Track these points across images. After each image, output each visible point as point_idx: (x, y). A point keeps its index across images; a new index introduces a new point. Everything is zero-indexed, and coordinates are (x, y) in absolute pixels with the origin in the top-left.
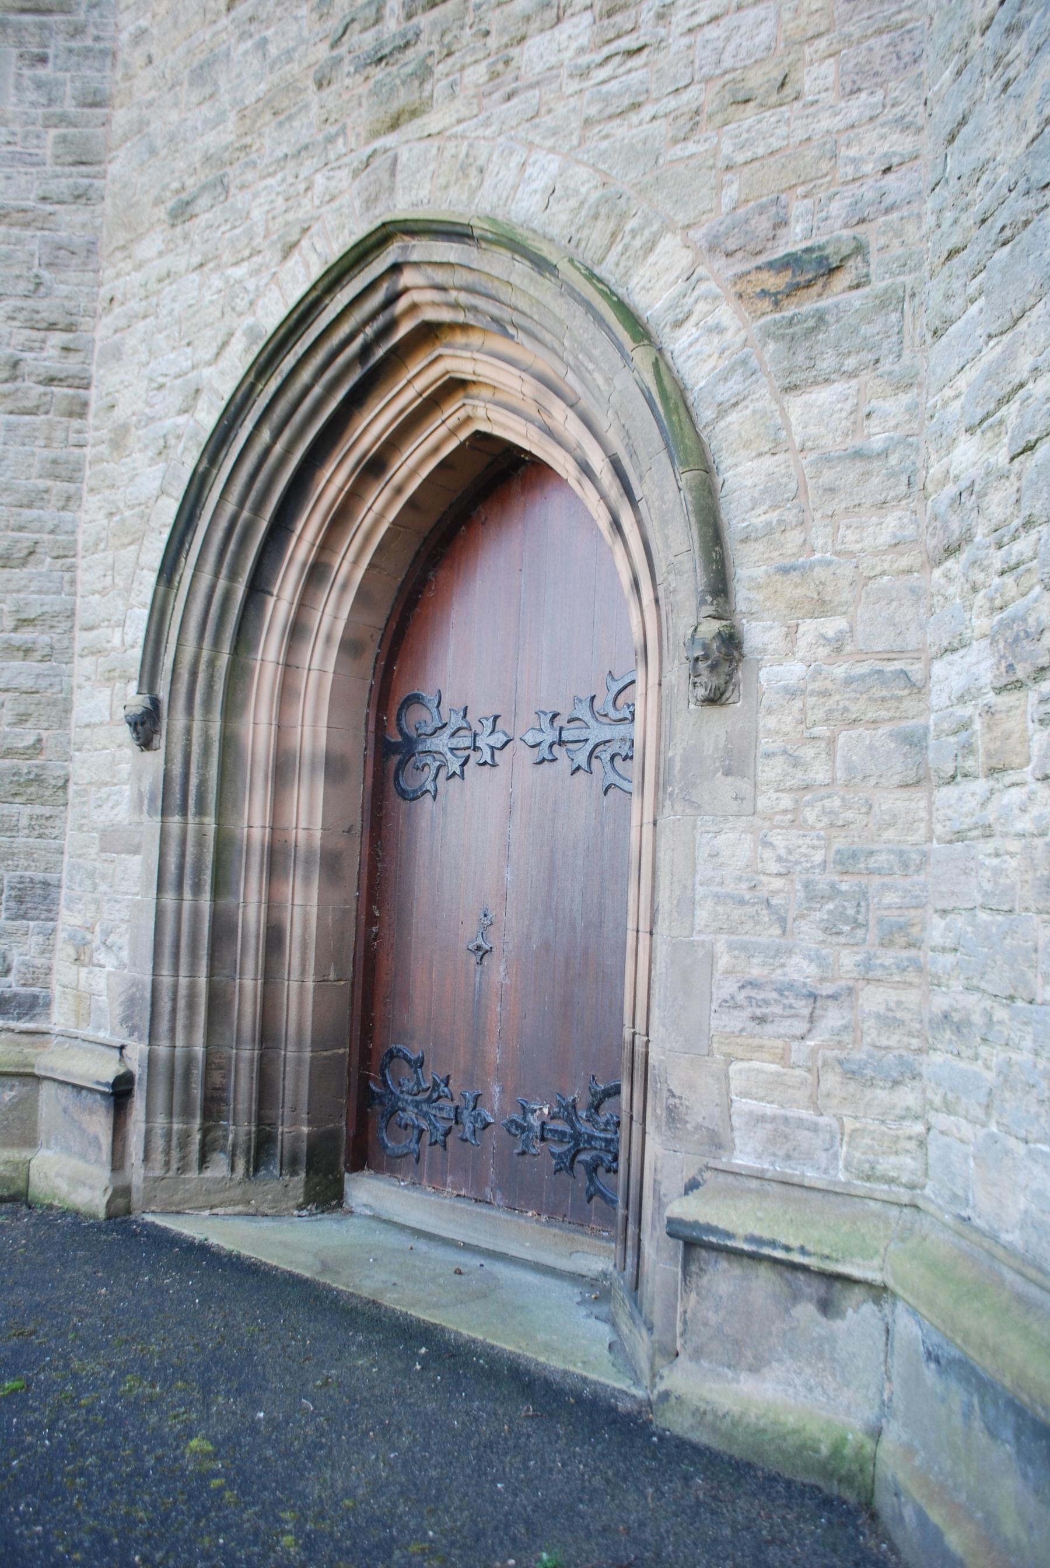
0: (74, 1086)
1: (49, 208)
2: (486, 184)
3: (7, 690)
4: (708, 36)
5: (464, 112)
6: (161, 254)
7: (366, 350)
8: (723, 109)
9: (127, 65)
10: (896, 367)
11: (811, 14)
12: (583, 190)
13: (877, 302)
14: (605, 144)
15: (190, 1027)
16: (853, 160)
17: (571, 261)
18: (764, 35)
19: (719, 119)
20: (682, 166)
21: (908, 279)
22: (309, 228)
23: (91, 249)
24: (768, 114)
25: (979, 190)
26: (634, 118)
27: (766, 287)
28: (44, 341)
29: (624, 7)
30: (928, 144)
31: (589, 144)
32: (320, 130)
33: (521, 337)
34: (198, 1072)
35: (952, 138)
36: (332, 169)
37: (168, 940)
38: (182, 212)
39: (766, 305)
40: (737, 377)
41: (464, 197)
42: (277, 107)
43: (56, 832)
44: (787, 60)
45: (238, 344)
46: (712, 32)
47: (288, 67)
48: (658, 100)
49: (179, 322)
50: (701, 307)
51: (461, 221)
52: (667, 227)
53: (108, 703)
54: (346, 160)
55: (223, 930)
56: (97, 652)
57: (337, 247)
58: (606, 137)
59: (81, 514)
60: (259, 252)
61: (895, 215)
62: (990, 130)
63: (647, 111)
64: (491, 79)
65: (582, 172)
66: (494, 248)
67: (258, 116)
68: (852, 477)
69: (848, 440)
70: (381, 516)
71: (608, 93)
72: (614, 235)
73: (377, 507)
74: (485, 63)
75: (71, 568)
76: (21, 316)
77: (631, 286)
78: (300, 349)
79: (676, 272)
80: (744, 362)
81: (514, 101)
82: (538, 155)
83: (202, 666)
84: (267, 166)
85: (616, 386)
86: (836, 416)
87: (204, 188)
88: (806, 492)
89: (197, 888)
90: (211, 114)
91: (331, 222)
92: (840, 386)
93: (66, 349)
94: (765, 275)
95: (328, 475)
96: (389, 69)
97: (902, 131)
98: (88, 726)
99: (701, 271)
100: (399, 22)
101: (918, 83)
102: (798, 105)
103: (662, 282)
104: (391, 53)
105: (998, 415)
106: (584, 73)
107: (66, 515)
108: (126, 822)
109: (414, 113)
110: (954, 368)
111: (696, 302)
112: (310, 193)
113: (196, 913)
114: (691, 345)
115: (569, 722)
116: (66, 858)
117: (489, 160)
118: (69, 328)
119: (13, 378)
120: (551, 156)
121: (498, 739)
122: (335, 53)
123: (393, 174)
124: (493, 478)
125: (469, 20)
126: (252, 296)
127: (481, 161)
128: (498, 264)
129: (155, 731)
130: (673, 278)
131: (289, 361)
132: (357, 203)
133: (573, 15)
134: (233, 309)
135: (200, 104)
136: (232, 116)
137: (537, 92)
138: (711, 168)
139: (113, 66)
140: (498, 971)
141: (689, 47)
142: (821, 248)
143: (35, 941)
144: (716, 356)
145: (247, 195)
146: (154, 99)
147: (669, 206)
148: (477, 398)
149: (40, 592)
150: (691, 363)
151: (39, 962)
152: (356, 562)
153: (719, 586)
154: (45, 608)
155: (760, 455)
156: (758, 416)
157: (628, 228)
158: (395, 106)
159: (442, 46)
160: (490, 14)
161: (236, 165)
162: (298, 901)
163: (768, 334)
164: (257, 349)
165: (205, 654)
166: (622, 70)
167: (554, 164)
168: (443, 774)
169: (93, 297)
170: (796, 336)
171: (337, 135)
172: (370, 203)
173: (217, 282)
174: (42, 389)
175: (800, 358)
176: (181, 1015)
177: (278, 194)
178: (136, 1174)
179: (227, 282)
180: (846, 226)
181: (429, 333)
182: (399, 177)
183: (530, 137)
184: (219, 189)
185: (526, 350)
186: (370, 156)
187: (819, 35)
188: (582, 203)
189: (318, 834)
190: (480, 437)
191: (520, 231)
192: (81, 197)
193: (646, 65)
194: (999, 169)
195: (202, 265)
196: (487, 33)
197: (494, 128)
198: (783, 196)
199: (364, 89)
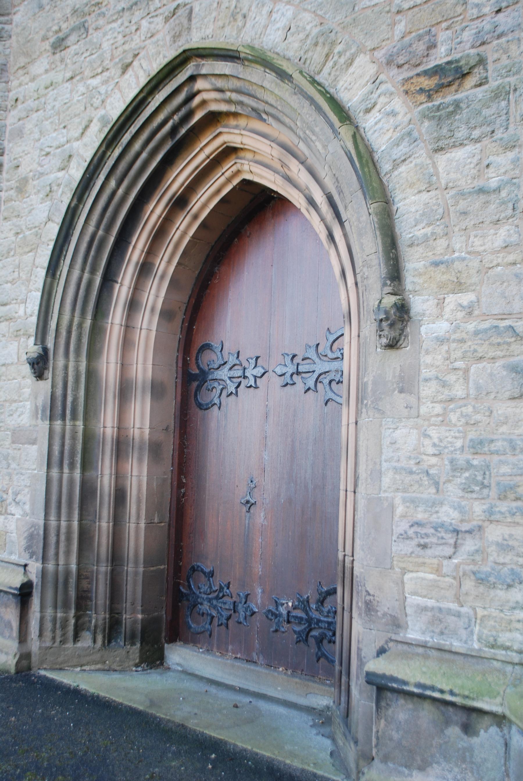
2: (248, 25)
6: (47, 71)
10: (505, 135)
12: (308, 27)
13: (493, 94)
15: (68, 553)
17: (301, 72)
20: (370, 11)
22: (138, 54)
33: (271, 120)
34: (73, 581)
36: (152, 17)
37: (54, 498)
38: (59, 45)
39: (423, 98)
40: (405, 143)
41: (234, 33)
45: (95, 127)
51: (232, 48)
52: (360, 50)
54: (161, 11)
55: (88, 492)
57: (156, 65)
60: (108, 69)
61: (503, 40)
65: (307, 16)
66: (253, 65)
68: (477, 205)
70: (185, 233)
72: (327, 56)
77: (338, 87)
78: (133, 129)
80: (409, 134)
83: (74, 328)
84: (112, 15)
85: (330, 150)
86: (467, 167)
87: (73, 30)
88: (449, 214)
92: (470, 148)
94: (422, 79)
95: (151, 208)
103: (357, 85)
108: (28, 425)
111: (379, 96)
112: (138, 32)
113: (71, 481)
114: (376, 124)
115: (303, 360)
120: (288, 7)
121: (259, 371)
123: (190, 19)
126: (103, 97)
127: (244, 11)
128: (256, 75)
131: (127, 137)
132: (168, 38)
134: (92, 105)
138: (388, 12)
140: (260, 517)
142: (457, 61)
144: (392, 130)
145: (100, 33)
147: (361, 37)
150: (376, 135)
152: (169, 262)
153: (395, 274)
155: (420, 192)
156: (418, 168)
157: (336, 51)
161: (93, 15)
162: (135, 473)
163: (424, 116)
164: (106, 130)
172: (176, 37)
173: (81, 88)
176: (62, 545)
177: (119, 33)
178: (34, 645)
179: (88, 88)
180: (473, 47)
181: (213, 119)
182: (194, 21)
184: (82, 30)
186: (175, 9)
188: (308, 36)
189: (147, 431)
190: (245, 183)
191: (269, 54)
195: (72, 78)
198: (433, 29)
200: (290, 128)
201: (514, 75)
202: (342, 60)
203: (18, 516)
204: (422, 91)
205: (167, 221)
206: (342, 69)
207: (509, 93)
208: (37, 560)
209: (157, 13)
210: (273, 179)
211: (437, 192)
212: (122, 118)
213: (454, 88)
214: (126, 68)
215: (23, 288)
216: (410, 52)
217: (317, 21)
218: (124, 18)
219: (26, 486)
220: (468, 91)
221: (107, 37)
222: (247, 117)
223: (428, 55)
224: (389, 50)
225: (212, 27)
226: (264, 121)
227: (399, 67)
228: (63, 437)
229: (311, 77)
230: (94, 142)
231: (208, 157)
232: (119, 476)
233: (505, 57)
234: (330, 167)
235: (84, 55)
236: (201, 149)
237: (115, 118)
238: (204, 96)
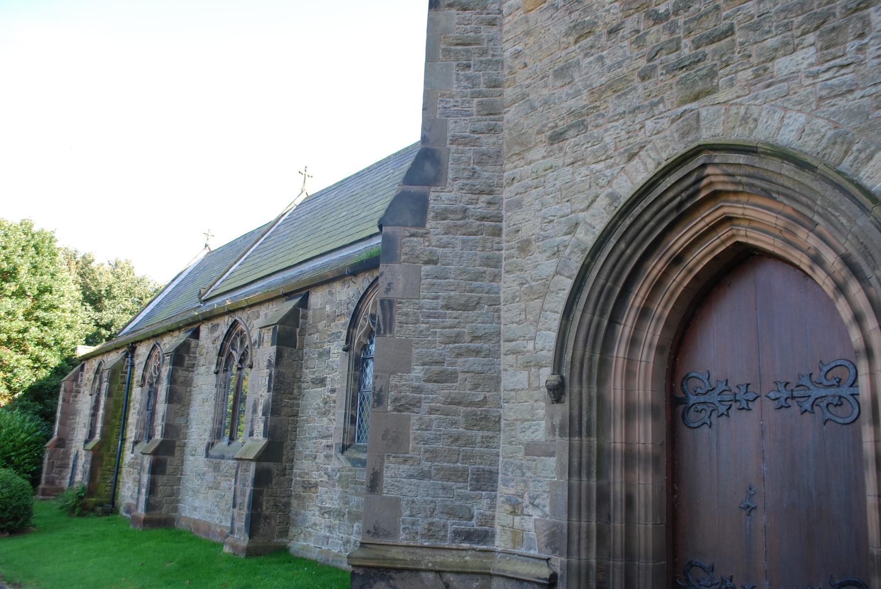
0: (517, 580)
1: (477, 136)
3: (468, 372)
5: (740, 93)
6: (544, 157)
9: (511, 68)
12: (823, 130)
14: (833, 109)
15: (588, 549)
23: (499, 154)
26: (850, 97)
28: (477, 200)
29: (836, 45)
34: (593, 573)
37: (575, 502)
38: (557, 137)
42: (617, 87)
43: (495, 445)
45: (602, 202)
49: (560, 190)
53: (526, 379)
55: (603, 497)
56: (515, 352)
58: (833, 105)
59: (502, 284)
63: (858, 94)
65: (822, 122)
67: (604, 92)
70: (680, 284)
71: (832, 85)
73: (678, 280)
75: (498, 310)
76: (467, 188)
83: (586, 361)
89: (589, 475)
93: (489, 203)
96: (687, 73)
98: (513, 390)
100: (691, 50)
104: (689, 65)
106: (815, 75)
107: (494, 284)
108: (543, 440)
109: (708, 93)
112: (643, 130)
113: (589, 488)
115: (797, 387)
116: (501, 459)
118: (490, 193)
119: (464, 218)
120: (799, 114)
121: (751, 396)
122: (651, 64)
124: (741, 259)
126: (609, 178)
128: (773, 165)
129: (563, 393)
132: (676, 135)
134: (597, 184)
139: (503, 68)
140: (761, 519)
143: (485, 502)
145: (600, 130)
149: (483, 323)
151: (488, 513)
152: (665, 307)
154: (486, 331)
158: (697, 89)
160: (750, 48)
161: (591, 116)
162: (642, 482)
165: (587, 354)
166: (838, 74)
168: (714, 414)
169: (500, 178)
172: (684, 135)
173: (584, 171)
174: (478, 223)
176: (583, 542)
181: (715, 195)
183: (785, 105)
188: (823, 136)
189: (650, 446)
192: (492, 130)
195: (573, 163)
196: (750, 56)
202: (863, 156)
203: (535, 517)
205: (665, 274)
208: (561, 555)
215: (532, 328)
217: (831, 125)
219: (544, 491)
226: (775, 199)
228: (581, 451)
231: (707, 225)
232: (629, 485)
236: (703, 219)
238: (713, 179)
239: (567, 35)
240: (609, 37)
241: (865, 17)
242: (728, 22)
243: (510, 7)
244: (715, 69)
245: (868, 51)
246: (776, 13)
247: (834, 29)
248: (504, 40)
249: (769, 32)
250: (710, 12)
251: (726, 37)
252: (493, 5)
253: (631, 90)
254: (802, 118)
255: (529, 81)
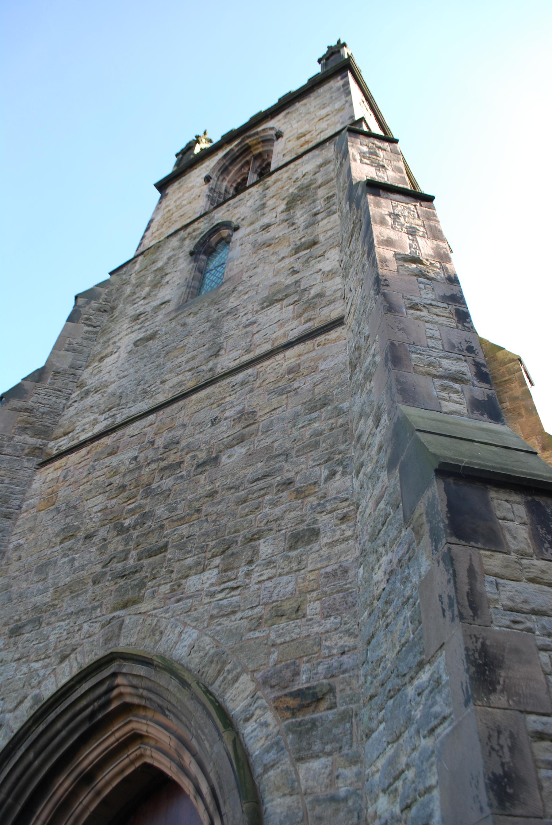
2: (163, 640)
4: (266, 586)
5: (157, 605)
7: (93, 714)
8: (271, 618)
9: (9, 559)
10: (350, 752)
11: (310, 581)
12: (207, 648)
13: (340, 717)
14: (219, 628)
16: (328, 647)
17: (198, 683)
18: (290, 588)
19: (270, 622)
20: (253, 642)
21: (354, 706)
22: (76, 649)
24: (291, 622)
25: (380, 669)
26: (233, 618)
27: (289, 705)
29: (232, 569)
30: (360, 643)
31: (212, 627)
32: (90, 603)
33: (172, 716)
35: (369, 643)
36: (92, 622)
39: (288, 714)
40: (274, 751)
41: (152, 644)
44: (300, 600)
45: (27, 703)
46: (268, 584)
47: (82, 572)
48: (244, 610)
50: (258, 712)
51: (148, 657)
52: (244, 670)
54: (100, 619)
57: (87, 660)
58: (220, 624)
60: (49, 657)
61: (347, 675)
62: (382, 643)
63: (239, 615)
64: (171, 592)
65: (207, 639)
66: (162, 671)
67: (63, 592)
68: (330, 812)
69: (328, 790)
70: (86, 807)
72: (219, 672)
73: (84, 803)
74: (170, 584)
77: (226, 697)
78: (59, 710)
79: (247, 693)
80: (277, 743)
81: (180, 603)
82: (188, 629)
84: (62, 616)
85: (215, 749)
86: (322, 776)
87: (30, 622)
88: (307, 818)
90: (42, 588)
91: (87, 648)
92: (323, 760)
94: (288, 699)
95: (60, 781)
96: (127, 581)
97: (349, 636)
99: (259, 693)
100: (134, 561)
101: (355, 615)
102: (304, 620)
103: (240, 697)
104: (129, 574)
105: (395, 785)
106: (212, 595)
109: (135, 602)
110: (375, 756)
111: (256, 709)
114: (252, 731)
117: (166, 629)
120: (194, 630)
122: (104, 570)
123: (120, 629)
125: (165, 565)
127: (162, 629)
128: (164, 680)
130: (245, 696)
131: (52, 716)
132: (101, 640)
133: (210, 569)
134: (30, 684)
135: (37, 582)
136: (51, 590)
137: (191, 600)
138: (266, 644)
141: (259, 589)
142: (314, 688)
144: (264, 738)
145: (50, 628)
146: (17, 576)
147: (245, 661)
148: (147, 744)
150: (252, 741)
155: (284, 795)
156: (284, 773)
157: (226, 669)
158: (126, 598)
159: (152, 574)
160: (174, 564)
161: (48, 613)
163: (289, 729)
164: (36, 708)
166: (229, 595)
167: (195, 634)
170: (303, 732)
171: (98, 607)
172: (107, 641)
175: (304, 744)
177: (65, 630)
179: (30, 670)
180: (325, 678)
181: (127, 709)
182: (123, 631)
184: (37, 623)
185: (173, 723)
186: (111, 619)
187: (313, 591)
188: (206, 654)
190: (147, 766)
191: (176, 665)
193: (239, 595)
194: (387, 662)
197: (170, 614)
198: (297, 661)
199: (113, 588)
200: (186, 726)
201: (355, 703)
204: (288, 708)
206: (229, 684)
207: (352, 717)
209: (97, 620)
210: (169, 766)
211: (299, 797)
212: (52, 700)
213: (312, 708)
214: (64, 658)
216: (280, 677)
217: (214, 644)
218: (71, 620)
220: (323, 713)
221: (55, 632)
222: (155, 711)
223: (293, 681)
224: (265, 673)
225: (136, 637)
227: (272, 687)
229: (205, 687)
230: (24, 716)
231: (117, 740)
233: (348, 688)
234: (214, 764)
235: (33, 643)
237: (45, 700)
238: (122, 689)
239: (57, 535)
240: (84, 541)
241: (256, 546)
242: (166, 539)
243: (28, 505)
244: (145, 580)
245: (253, 577)
246: (199, 536)
247: (233, 554)
248: (14, 533)
249: (190, 552)
250: (156, 529)
251: (161, 553)
252: (15, 501)
253: (82, 593)
254: (195, 634)
255: (17, 573)
